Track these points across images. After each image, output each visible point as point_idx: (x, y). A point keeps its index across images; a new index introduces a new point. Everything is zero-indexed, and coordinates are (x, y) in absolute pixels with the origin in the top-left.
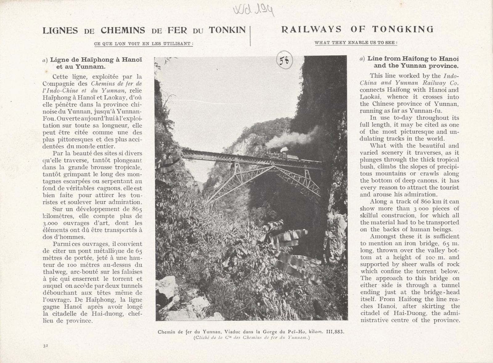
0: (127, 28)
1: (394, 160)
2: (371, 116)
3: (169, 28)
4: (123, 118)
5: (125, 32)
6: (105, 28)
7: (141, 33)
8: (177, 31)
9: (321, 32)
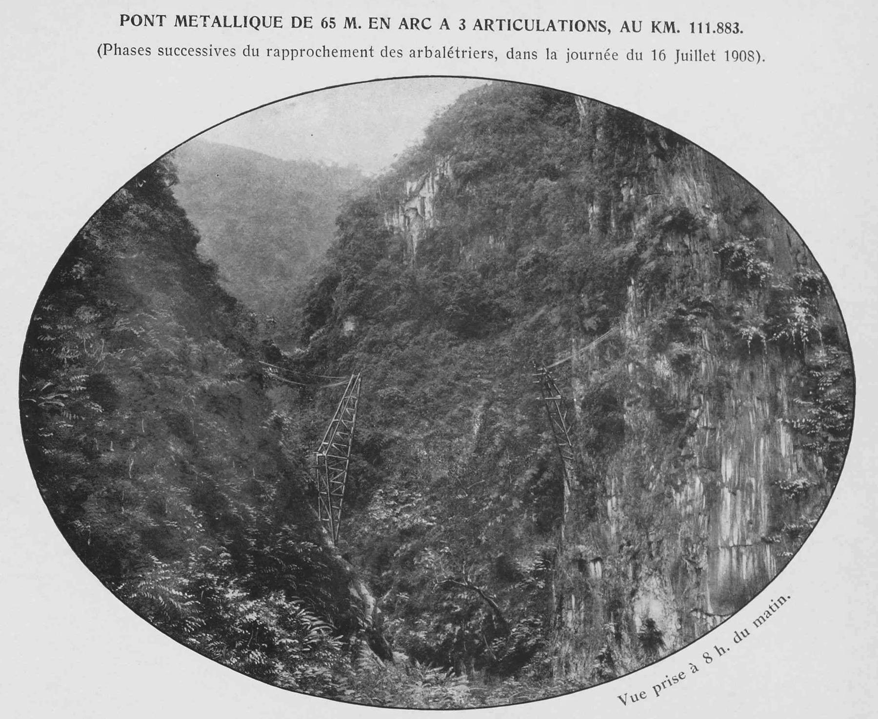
0: (184, 17)
1: (310, 52)
2: (678, 51)
3: (371, 19)
4: (222, 51)
5: (350, 27)
6: (521, 21)
7: (600, 30)
8: (374, 25)
9: (474, 29)
